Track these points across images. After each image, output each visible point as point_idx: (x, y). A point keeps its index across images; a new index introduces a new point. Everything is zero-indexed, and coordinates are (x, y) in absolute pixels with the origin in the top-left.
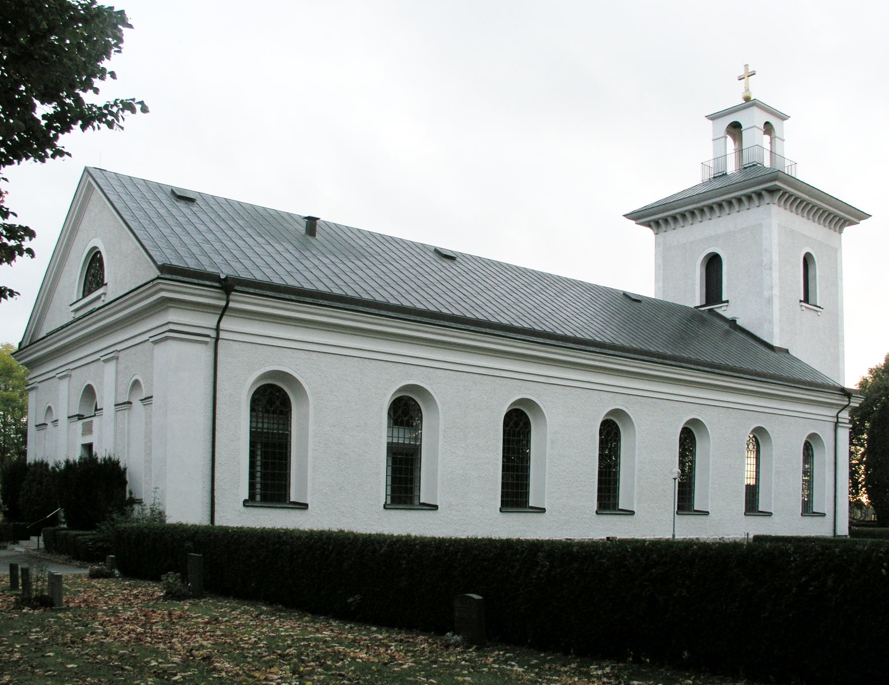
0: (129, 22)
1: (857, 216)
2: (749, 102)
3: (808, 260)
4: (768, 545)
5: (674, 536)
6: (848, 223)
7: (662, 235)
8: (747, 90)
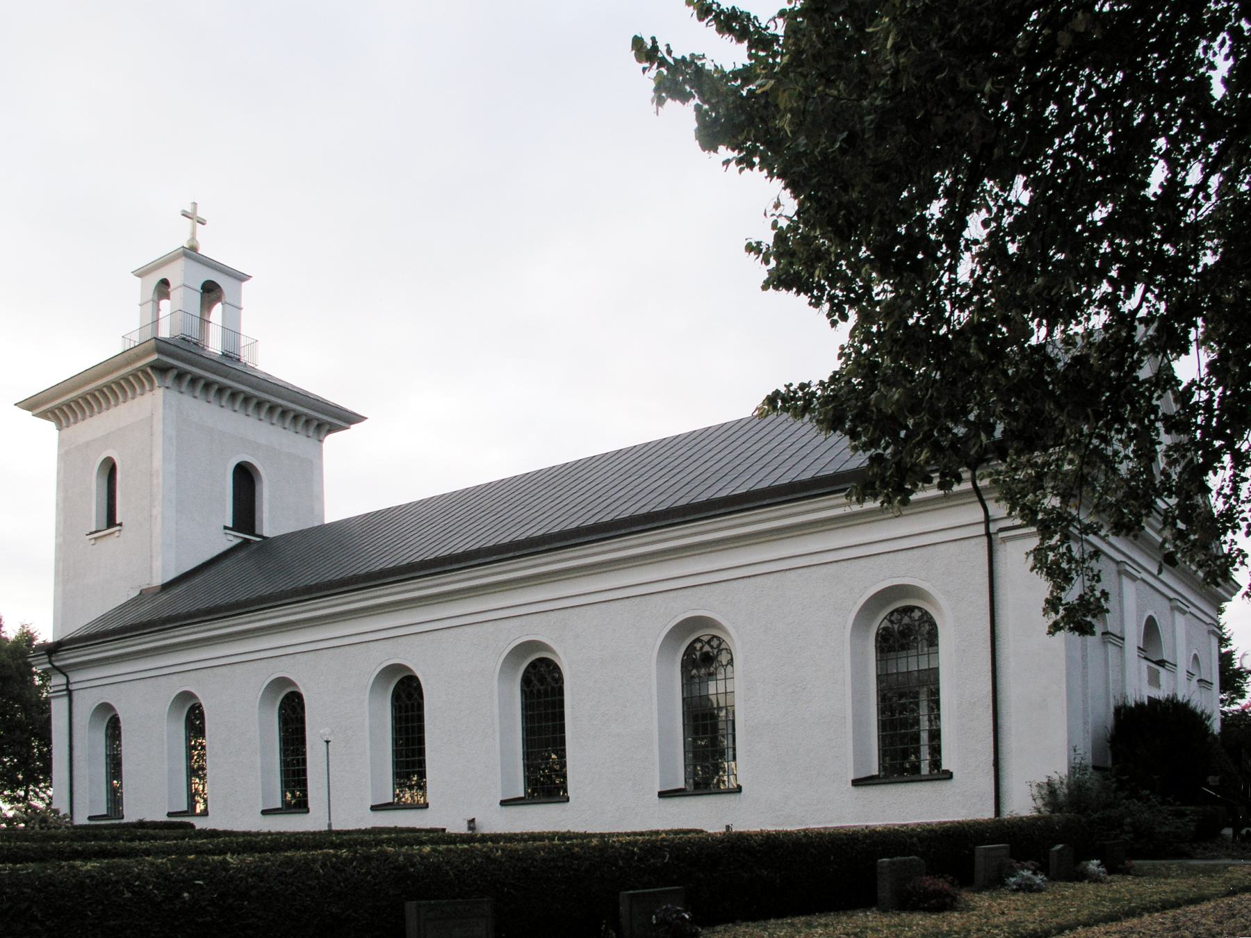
0: (776, 200)
1: (341, 419)
2: (191, 253)
3: (110, 470)
4: (241, 840)
5: (330, 825)
6: (327, 427)
7: (66, 431)
8: (193, 238)
